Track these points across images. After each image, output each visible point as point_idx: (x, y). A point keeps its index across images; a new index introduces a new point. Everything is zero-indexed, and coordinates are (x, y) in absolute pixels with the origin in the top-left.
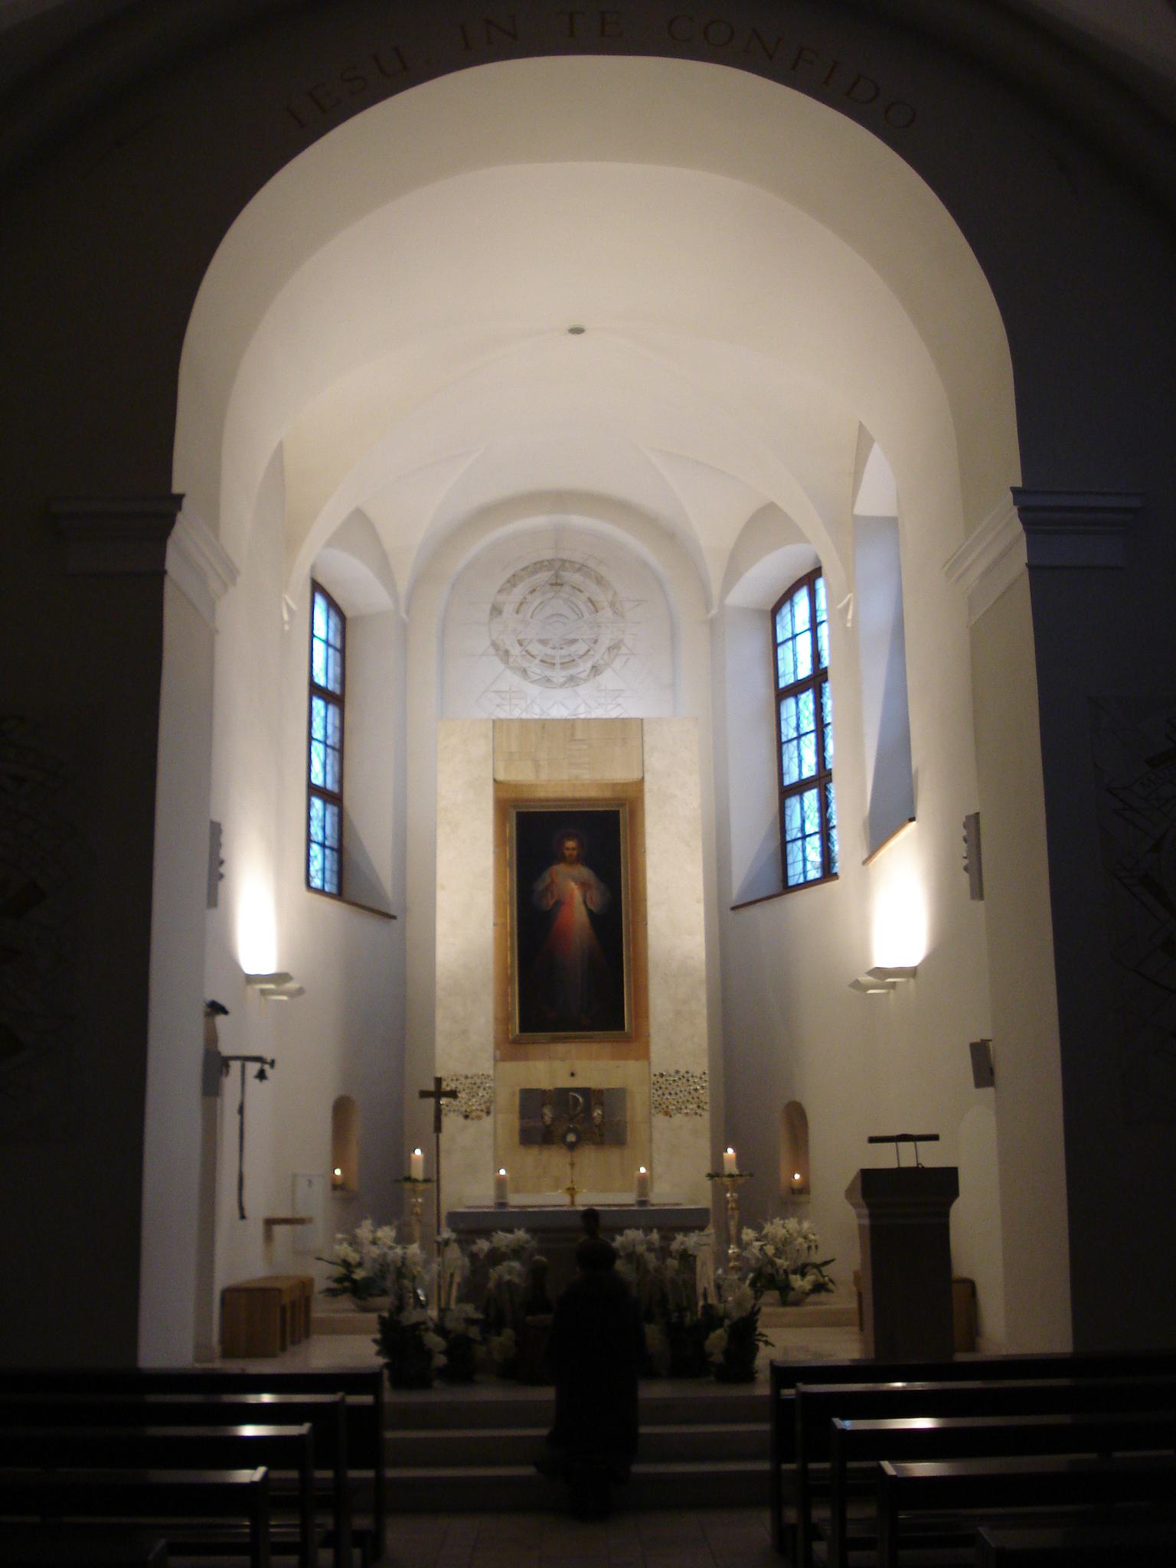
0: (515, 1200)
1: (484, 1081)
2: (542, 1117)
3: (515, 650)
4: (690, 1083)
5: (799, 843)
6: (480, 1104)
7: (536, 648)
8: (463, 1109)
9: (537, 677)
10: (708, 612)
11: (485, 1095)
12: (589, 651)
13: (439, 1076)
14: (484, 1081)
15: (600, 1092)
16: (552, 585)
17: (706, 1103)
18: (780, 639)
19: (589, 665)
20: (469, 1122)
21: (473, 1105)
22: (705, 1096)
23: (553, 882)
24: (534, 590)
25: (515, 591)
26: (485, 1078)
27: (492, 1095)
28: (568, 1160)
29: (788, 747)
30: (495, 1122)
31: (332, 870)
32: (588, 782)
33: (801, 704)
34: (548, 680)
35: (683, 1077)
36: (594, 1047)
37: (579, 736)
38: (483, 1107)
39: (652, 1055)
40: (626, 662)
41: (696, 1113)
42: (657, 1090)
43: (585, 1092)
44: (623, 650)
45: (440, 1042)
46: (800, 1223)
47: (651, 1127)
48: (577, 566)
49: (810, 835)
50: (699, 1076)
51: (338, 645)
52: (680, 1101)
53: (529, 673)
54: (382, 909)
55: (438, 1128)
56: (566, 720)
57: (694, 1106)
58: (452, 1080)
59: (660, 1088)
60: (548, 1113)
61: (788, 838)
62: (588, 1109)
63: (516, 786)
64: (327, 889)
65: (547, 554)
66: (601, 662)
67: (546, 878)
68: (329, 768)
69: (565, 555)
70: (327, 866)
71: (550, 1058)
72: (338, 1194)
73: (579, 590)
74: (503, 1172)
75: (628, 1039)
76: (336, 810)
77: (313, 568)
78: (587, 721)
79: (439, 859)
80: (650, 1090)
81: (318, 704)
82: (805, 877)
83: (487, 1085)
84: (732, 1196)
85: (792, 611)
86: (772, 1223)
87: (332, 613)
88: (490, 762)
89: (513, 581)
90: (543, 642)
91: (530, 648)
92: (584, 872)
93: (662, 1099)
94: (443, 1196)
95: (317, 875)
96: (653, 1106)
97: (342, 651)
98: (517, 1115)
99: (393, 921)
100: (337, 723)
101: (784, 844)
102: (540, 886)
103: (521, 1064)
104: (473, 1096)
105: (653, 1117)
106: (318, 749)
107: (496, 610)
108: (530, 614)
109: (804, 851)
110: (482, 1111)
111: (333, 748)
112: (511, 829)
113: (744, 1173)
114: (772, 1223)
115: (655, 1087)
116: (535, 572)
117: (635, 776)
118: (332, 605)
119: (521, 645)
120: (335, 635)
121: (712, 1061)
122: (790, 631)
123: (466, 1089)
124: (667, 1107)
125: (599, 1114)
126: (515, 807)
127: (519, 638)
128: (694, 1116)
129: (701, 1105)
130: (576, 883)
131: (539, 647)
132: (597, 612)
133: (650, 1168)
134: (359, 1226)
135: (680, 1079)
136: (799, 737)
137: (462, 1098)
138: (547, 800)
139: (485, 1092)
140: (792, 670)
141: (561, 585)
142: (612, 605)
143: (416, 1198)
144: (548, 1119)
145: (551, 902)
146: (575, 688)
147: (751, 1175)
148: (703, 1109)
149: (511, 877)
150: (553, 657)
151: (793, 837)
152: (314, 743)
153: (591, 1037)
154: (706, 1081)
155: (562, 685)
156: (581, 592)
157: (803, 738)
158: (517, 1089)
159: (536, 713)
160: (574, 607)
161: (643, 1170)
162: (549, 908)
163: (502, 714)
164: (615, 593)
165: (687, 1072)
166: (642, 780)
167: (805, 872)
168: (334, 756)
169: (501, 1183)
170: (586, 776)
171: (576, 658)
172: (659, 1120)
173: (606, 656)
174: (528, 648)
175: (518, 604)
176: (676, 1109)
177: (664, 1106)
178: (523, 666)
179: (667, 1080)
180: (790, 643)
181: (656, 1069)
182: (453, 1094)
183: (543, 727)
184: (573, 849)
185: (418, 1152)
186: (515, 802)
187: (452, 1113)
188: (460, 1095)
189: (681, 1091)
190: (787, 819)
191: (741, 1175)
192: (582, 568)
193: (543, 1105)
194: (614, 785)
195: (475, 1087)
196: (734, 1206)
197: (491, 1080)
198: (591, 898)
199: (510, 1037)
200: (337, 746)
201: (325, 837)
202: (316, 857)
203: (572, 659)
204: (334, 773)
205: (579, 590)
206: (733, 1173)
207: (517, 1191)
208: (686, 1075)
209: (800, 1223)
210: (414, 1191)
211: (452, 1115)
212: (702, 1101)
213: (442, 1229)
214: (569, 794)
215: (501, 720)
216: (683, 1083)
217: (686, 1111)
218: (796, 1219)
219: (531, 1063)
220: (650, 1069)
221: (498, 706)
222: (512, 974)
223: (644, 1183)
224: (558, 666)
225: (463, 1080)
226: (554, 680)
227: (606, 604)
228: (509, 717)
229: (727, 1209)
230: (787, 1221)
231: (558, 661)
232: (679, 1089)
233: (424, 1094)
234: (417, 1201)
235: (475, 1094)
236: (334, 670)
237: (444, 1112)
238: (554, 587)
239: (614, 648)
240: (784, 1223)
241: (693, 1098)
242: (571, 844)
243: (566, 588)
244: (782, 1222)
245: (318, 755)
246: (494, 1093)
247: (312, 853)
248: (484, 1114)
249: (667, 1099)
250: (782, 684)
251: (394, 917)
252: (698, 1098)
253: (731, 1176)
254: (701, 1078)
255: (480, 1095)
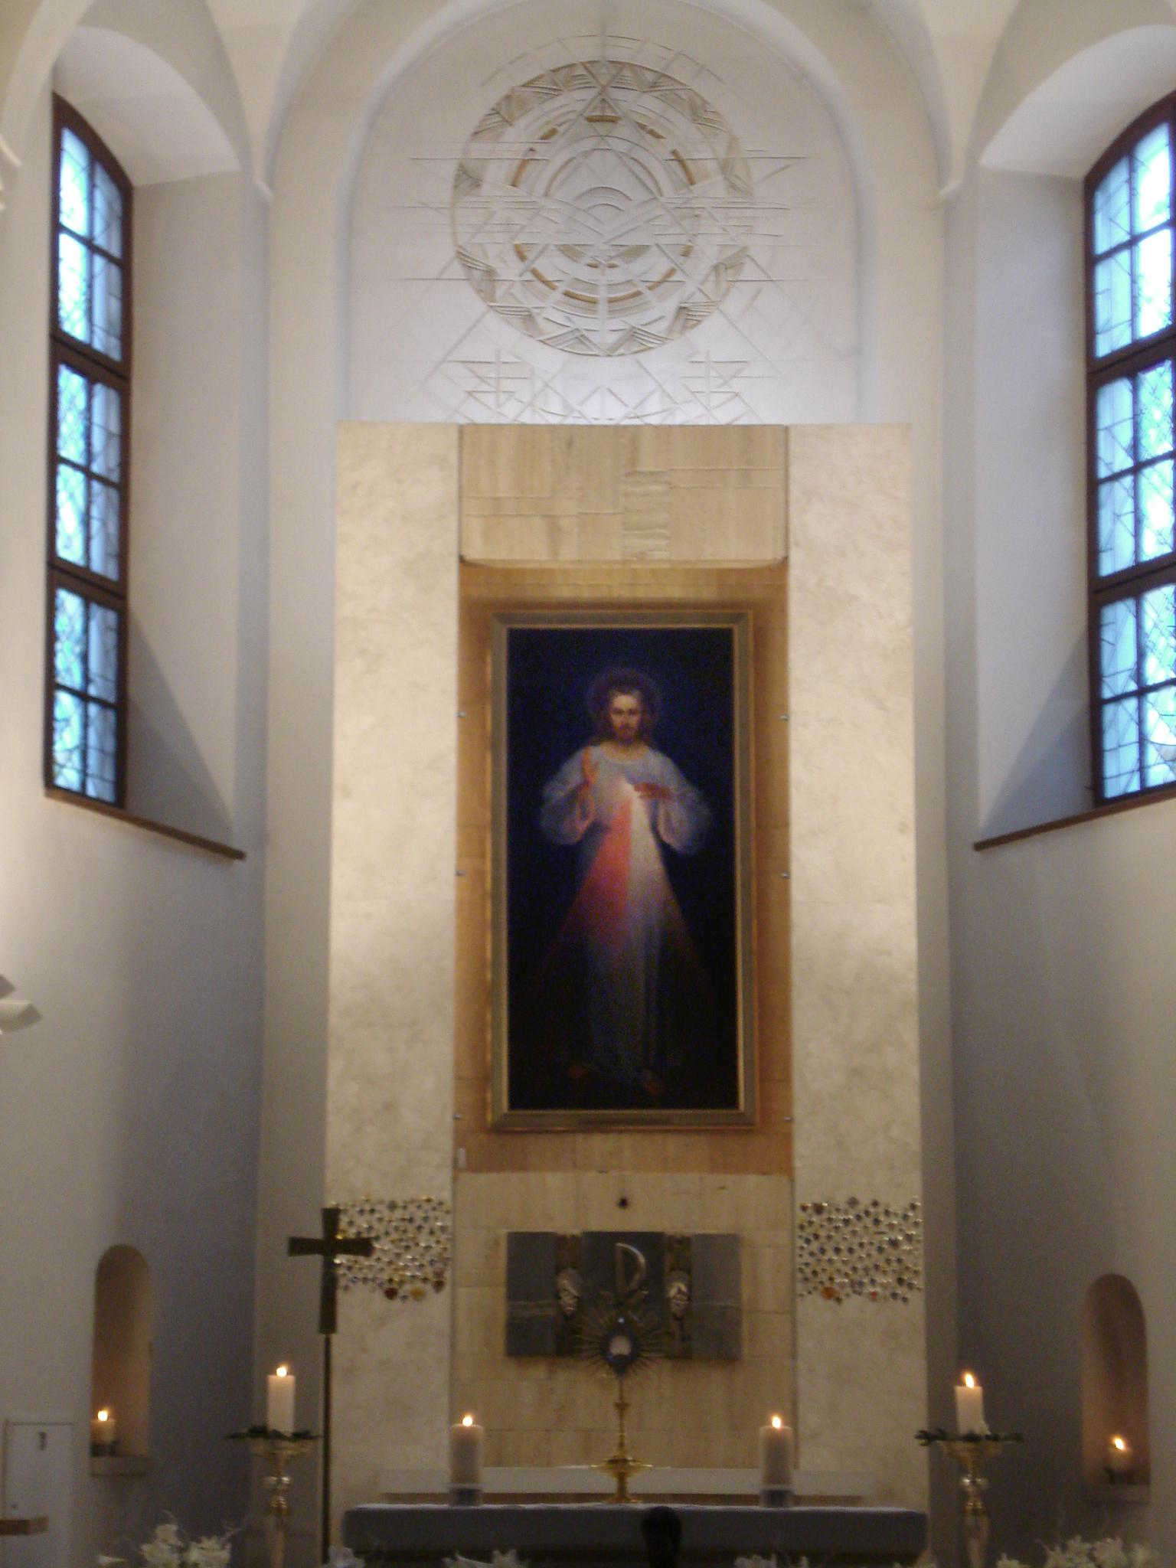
0: (493, 1480)
1: (432, 1214)
2: (558, 1297)
3: (510, 270)
4: (882, 1228)
5: (1131, 704)
6: (422, 1266)
7: (553, 266)
8: (385, 1276)
9: (613, 338)
10: (940, 183)
11: (433, 1245)
12: (672, 272)
13: (331, 1203)
14: (432, 1214)
15: (684, 1242)
16: (591, 120)
17: (916, 1272)
18: (1102, 246)
19: (672, 304)
20: (397, 1303)
21: (406, 1267)
22: (915, 1256)
23: (586, 783)
24: (553, 132)
25: (511, 133)
26: (434, 1209)
27: (449, 1246)
28: (614, 1397)
29: (1111, 490)
30: (454, 1308)
31: (102, 751)
32: (667, 566)
33: (1145, 394)
34: (581, 338)
35: (867, 1213)
36: (673, 1144)
37: (647, 464)
38: (429, 1271)
39: (798, 1163)
40: (756, 296)
41: (894, 1295)
42: (808, 1241)
43: (651, 1241)
44: (748, 272)
45: (337, 1130)
46: (1127, 1548)
47: (794, 1323)
48: (650, 77)
49: (1156, 688)
50: (900, 1212)
51: (115, 251)
52: (859, 1266)
53: (539, 320)
54: (217, 838)
55: (328, 1321)
56: (619, 430)
57: (890, 1279)
58: (362, 1212)
59: (816, 1237)
60: (569, 1287)
61: (1107, 694)
62: (656, 1279)
63: (508, 574)
64: (91, 791)
65: (585, 52)
66: (699, 298)
67: (571, 774)
68: (95, 525)
69: (622, 53)
70: (93, 740)
71: (575, 1165)
72: (104, 1463)
73: (652, 133)
74: (468, 1421)
75: (746, 1127)
76: (112, 617)
77: (57, 72)
78: (664, 432)
79: (337, 731)
80: (793, 1244)
81: (71, 383)
82: (1143, 780)
83: (439, 1224)
84: (973, 1482)
85: (1131, 182)
86: (1064, 1548)
87: (101, 177)
88: (452, 523)
89: (504, 112)
90: (571, 252)
91: (540, 265)
92: (653, 763)
93: (819, 1260)
94: (336, 1470)
95: (69, 759)
96: (799, 1276)
97: (124, 264)
98: (502, 1291)
99: (237, 863)
100: (114, 426)
101: (1096, 705)
102: (557, 792)
103: (515, 1178)
104: (407, 1248)
105: (799, 1300)
106: (70, 484)
107: (468, 178)
108: (540, 189)
109: (1141, 722)
110: (425, 1280)
111: (104, 481)
112: (496, 666)
113: (1002, 1434)
114: (1064, 1548)
115: (804, 1235)
116: (554, 92)
117: (769, 554)
118: (100, 156)
119: (522, 257)
120: (108, 226)
121: (929, 1184)
122: (1127, 227)
123: (391, 1230)
124: (831, 1279)
125: (680, 1291)
126: (504, 618)
127: (517, 242)
128: (891, 1300)
129: (905, 1277)
130: (632, 780)
131: (563, 262)
132: (692, 183)
133: (792, 1417)
134: (149, 1538)
135: (858, 1218)
136: (1137, 468)
137: (383, 1251)
138: (574, 605)
139: (434, 1238)
140: (1127, 316)
141: (613, 120)
142: (725, 167)
143: (279, 1474)
144: (568, 1301)
145: (582, 826)
146: (640, 356)
147: (1018, 1438)
148: (910, 1286)
149: (494, 770)
150: (593, 286)
151: (1119, 691)
152: (63, 469)
153: (666, 1122)
154: (916, 1224)
155: (611, 352)
156: (658, 137)
157: (1148, 471)
158: (503, 1232)
159: (551, 412)
160: (638, 170)
161: (777, 1422)
162: (575, 839)
163: (479, 414)
164: (733, 143)
165: (875, 1204)
166: (781, 567)
167: (1142, 768)
168: (108, 497)
169: (464, 1444)
170: (661, 552)
171: (642, 288)
172: (812, 1308)
173: (709, 288)
174: (538, 265)
175: (516, 164)
176: (852, 1284)
177: (824, 1277)
178: (527, 305)
179: (830, 1220)
180: (1124, 257)
181: (807, 1195)
182: (362, 1246)
183: (570, 444)
184: (631, 712)
185: (282, 1372)
186: (503, 610)
187: (360, 1285)
188: (377, 1245)
189: (861, 1245)
190: (1106, 650)
191: (995, 1438)
192: (658, 83)
193: (558, 1270)
194: (722, 574)
195: (411, 1228)
196: (979, 1505)
197: (448, 1212)
198: (668, 820)
199: (489, 1117)
200: (115, 477)
201: (87, 678)
202: (67, 721)
203: (633, 290)
204: (107, 537)
205: (652, 133)
206: (977, 1431)
207: (499, 1462)
208: (872, 1210)
209: (1127, 1548)
210: (273, 1457)
211: (360, 1292)
212: (907, 1268)
213: (333, 1549)
214: (622, 592)
215: (477, 426)
216: (866, 1227)
217: (872, 1290)
218: (1119, 1540)
219: (533, 1177)
220: (792, 1193)
221: (470, 393)
222: (495, 981)
223: (778, 1451)
224: (603, 307)
225: (386, 1213)
226: (595, 338)
227: (712, 166)
228: (493, 421)
229: (963, 1512)
230: (1098, 1544)
231: (602, 295)
232: (857, 1240)
233: (299, 1246)
234: (280, 1481)
235: (411, 1244)
236: (106, 307)
237: (342, 1282)
238: (598, 126)
239: (727, 267)
240: (1093, 1549)
241: (888, 1261)
242: (625, 701)
243: (623, 130)
244: (1087, 1546)
245: (72, 496)
246: (453, 1240)
247: (59, 713)
248: (429, 1288)
249: (830, 1261)
250: (1103, 349)
251: (239, 855)
252: (899, 1261)
253: (972, 1438)
254: (906, 1217)
255: (423, 1244)
